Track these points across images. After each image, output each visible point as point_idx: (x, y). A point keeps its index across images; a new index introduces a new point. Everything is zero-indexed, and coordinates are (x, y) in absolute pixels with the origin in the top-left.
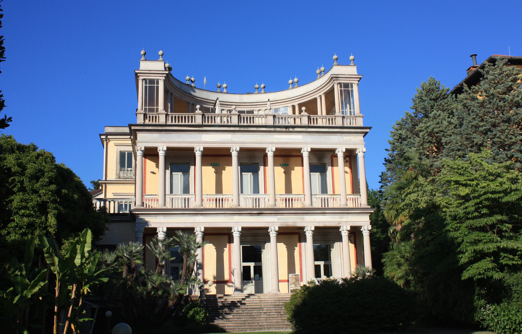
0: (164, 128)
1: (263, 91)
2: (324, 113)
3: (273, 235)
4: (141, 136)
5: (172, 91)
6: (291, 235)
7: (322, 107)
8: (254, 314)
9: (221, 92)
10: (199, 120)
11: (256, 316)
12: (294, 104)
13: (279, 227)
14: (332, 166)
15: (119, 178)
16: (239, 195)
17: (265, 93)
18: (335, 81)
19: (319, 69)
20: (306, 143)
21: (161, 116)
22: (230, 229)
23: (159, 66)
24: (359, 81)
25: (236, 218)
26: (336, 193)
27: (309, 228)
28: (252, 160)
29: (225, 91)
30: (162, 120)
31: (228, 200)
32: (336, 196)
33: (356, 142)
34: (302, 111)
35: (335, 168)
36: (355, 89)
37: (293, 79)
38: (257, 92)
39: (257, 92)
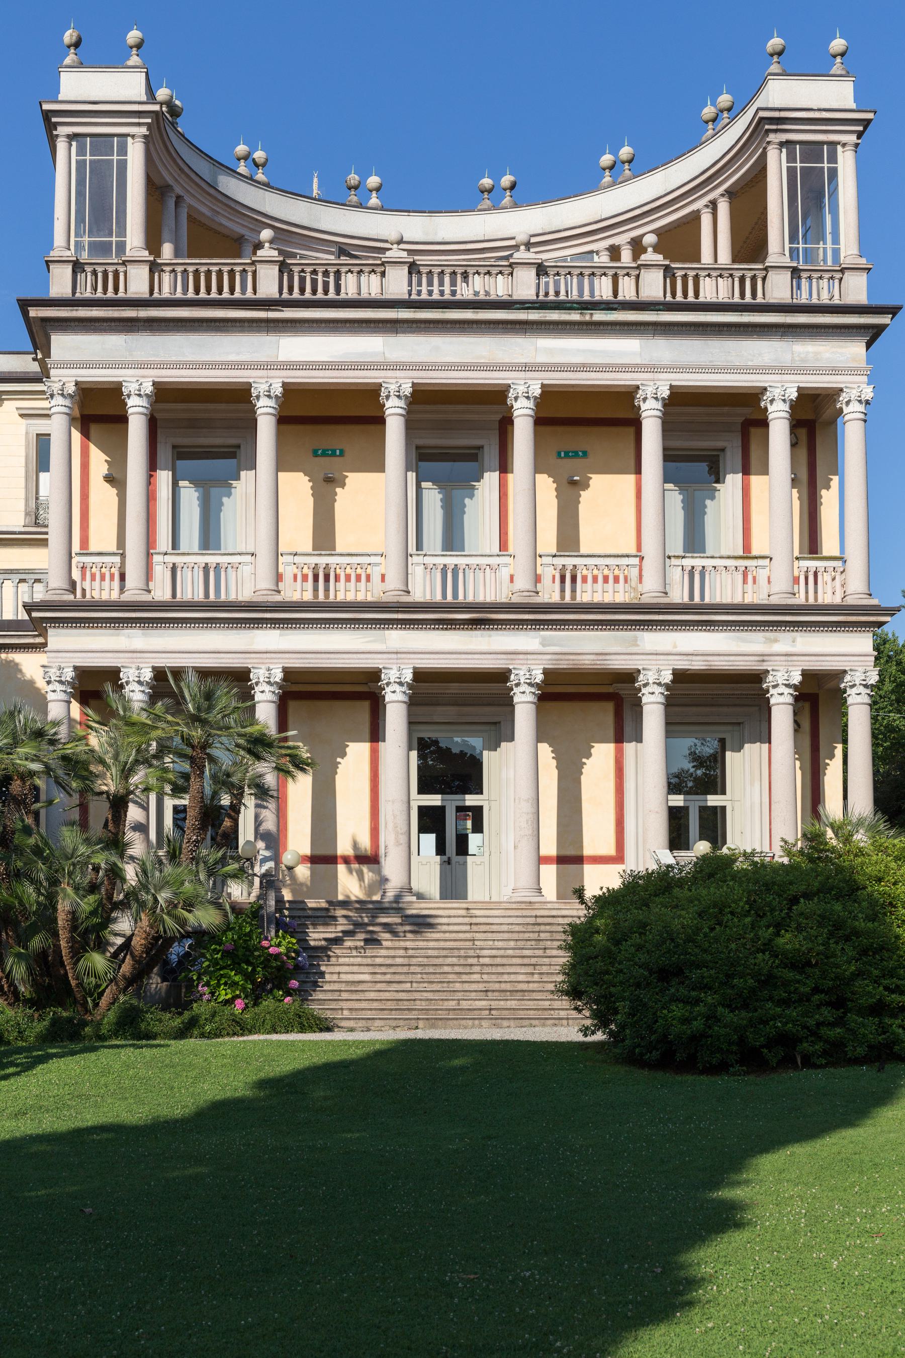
0: (144, 313)
1: (507, 200)
2: (725, 257)
3: (524, 703)
4: (62, 344)
5: (178, 190)
6: (590, 701)
7: (716, 241)
8: (446, 969)
9: (361, 206)
10: (268, 284)
11: (452, 977)
12: (615, 241)
13: (546, 672)
14: (746, 471)
15: (37, 524)
16: (407, 555)
17: (516, 205)
18: (772, 137)
19: (714, 104)
20: (653, 368)
21: (132, 270)
22: (374, 675)
23: (124, 85)
24: (860, 135)
25: (397, 638)
26: (755, 552)
27: (651, 677)
28: (457, 434)
29: (374, 201)
30: (137, 283)
31: (368, 578)
32: (754, 563)
33: (838, 363)
34: (645, 251)
35: (755, 480)
36: (846, 163)
37: (615, 152)
38: (487, 203)
39: (487, 203)
